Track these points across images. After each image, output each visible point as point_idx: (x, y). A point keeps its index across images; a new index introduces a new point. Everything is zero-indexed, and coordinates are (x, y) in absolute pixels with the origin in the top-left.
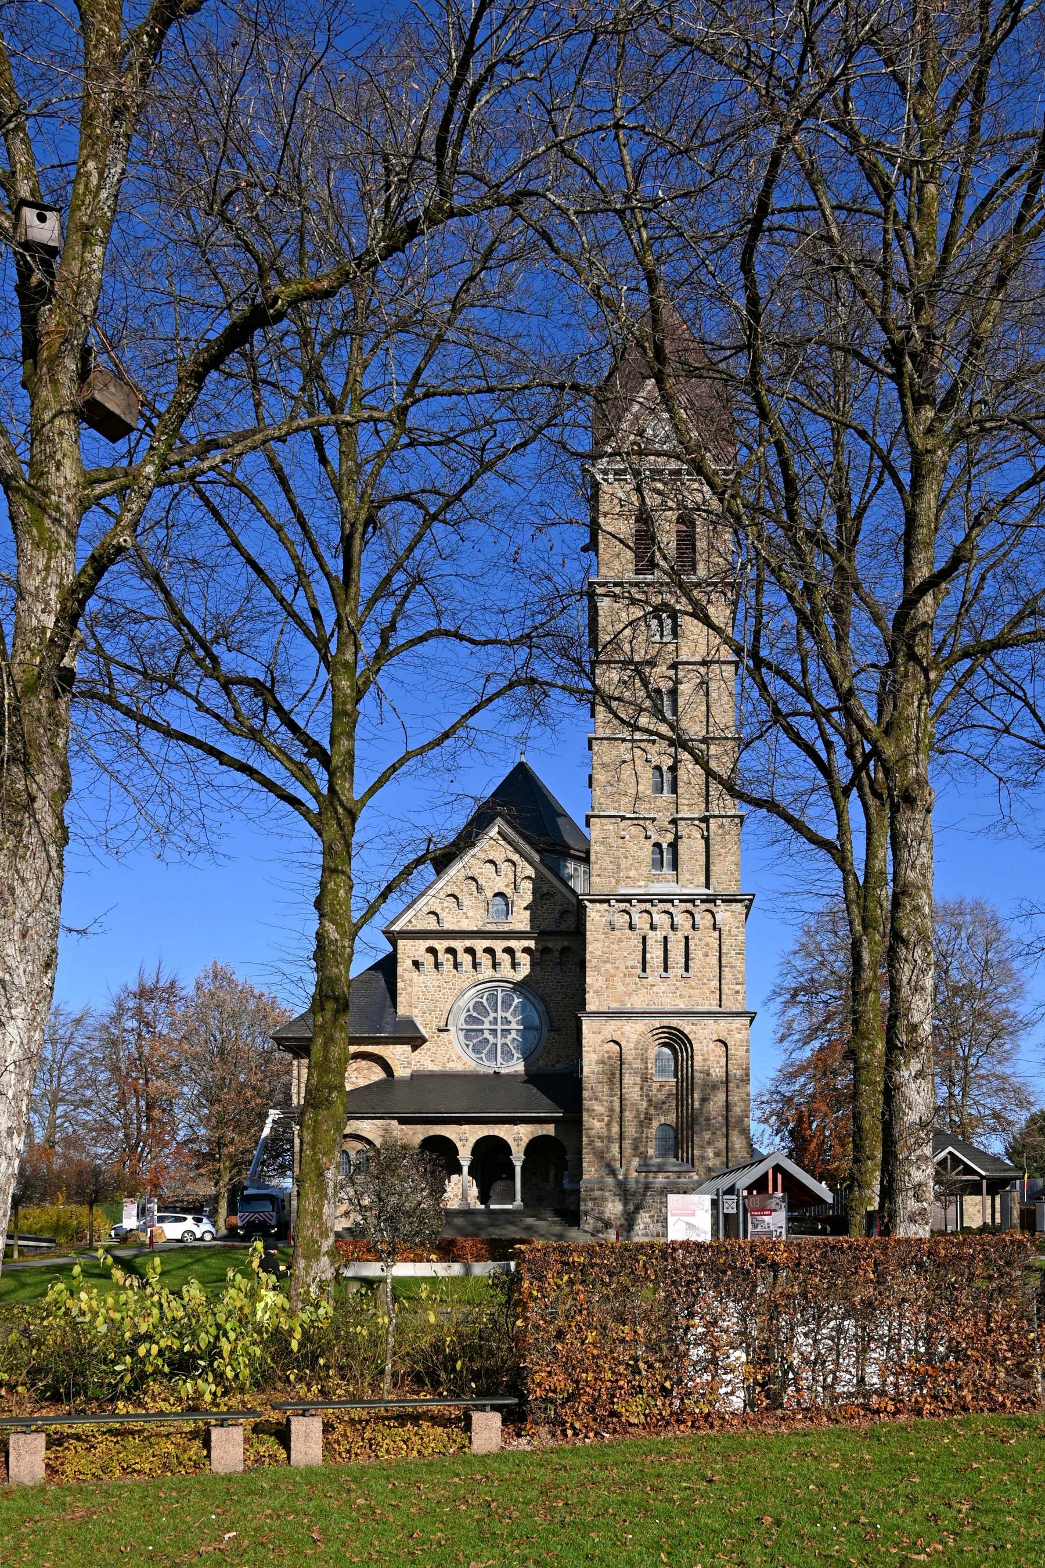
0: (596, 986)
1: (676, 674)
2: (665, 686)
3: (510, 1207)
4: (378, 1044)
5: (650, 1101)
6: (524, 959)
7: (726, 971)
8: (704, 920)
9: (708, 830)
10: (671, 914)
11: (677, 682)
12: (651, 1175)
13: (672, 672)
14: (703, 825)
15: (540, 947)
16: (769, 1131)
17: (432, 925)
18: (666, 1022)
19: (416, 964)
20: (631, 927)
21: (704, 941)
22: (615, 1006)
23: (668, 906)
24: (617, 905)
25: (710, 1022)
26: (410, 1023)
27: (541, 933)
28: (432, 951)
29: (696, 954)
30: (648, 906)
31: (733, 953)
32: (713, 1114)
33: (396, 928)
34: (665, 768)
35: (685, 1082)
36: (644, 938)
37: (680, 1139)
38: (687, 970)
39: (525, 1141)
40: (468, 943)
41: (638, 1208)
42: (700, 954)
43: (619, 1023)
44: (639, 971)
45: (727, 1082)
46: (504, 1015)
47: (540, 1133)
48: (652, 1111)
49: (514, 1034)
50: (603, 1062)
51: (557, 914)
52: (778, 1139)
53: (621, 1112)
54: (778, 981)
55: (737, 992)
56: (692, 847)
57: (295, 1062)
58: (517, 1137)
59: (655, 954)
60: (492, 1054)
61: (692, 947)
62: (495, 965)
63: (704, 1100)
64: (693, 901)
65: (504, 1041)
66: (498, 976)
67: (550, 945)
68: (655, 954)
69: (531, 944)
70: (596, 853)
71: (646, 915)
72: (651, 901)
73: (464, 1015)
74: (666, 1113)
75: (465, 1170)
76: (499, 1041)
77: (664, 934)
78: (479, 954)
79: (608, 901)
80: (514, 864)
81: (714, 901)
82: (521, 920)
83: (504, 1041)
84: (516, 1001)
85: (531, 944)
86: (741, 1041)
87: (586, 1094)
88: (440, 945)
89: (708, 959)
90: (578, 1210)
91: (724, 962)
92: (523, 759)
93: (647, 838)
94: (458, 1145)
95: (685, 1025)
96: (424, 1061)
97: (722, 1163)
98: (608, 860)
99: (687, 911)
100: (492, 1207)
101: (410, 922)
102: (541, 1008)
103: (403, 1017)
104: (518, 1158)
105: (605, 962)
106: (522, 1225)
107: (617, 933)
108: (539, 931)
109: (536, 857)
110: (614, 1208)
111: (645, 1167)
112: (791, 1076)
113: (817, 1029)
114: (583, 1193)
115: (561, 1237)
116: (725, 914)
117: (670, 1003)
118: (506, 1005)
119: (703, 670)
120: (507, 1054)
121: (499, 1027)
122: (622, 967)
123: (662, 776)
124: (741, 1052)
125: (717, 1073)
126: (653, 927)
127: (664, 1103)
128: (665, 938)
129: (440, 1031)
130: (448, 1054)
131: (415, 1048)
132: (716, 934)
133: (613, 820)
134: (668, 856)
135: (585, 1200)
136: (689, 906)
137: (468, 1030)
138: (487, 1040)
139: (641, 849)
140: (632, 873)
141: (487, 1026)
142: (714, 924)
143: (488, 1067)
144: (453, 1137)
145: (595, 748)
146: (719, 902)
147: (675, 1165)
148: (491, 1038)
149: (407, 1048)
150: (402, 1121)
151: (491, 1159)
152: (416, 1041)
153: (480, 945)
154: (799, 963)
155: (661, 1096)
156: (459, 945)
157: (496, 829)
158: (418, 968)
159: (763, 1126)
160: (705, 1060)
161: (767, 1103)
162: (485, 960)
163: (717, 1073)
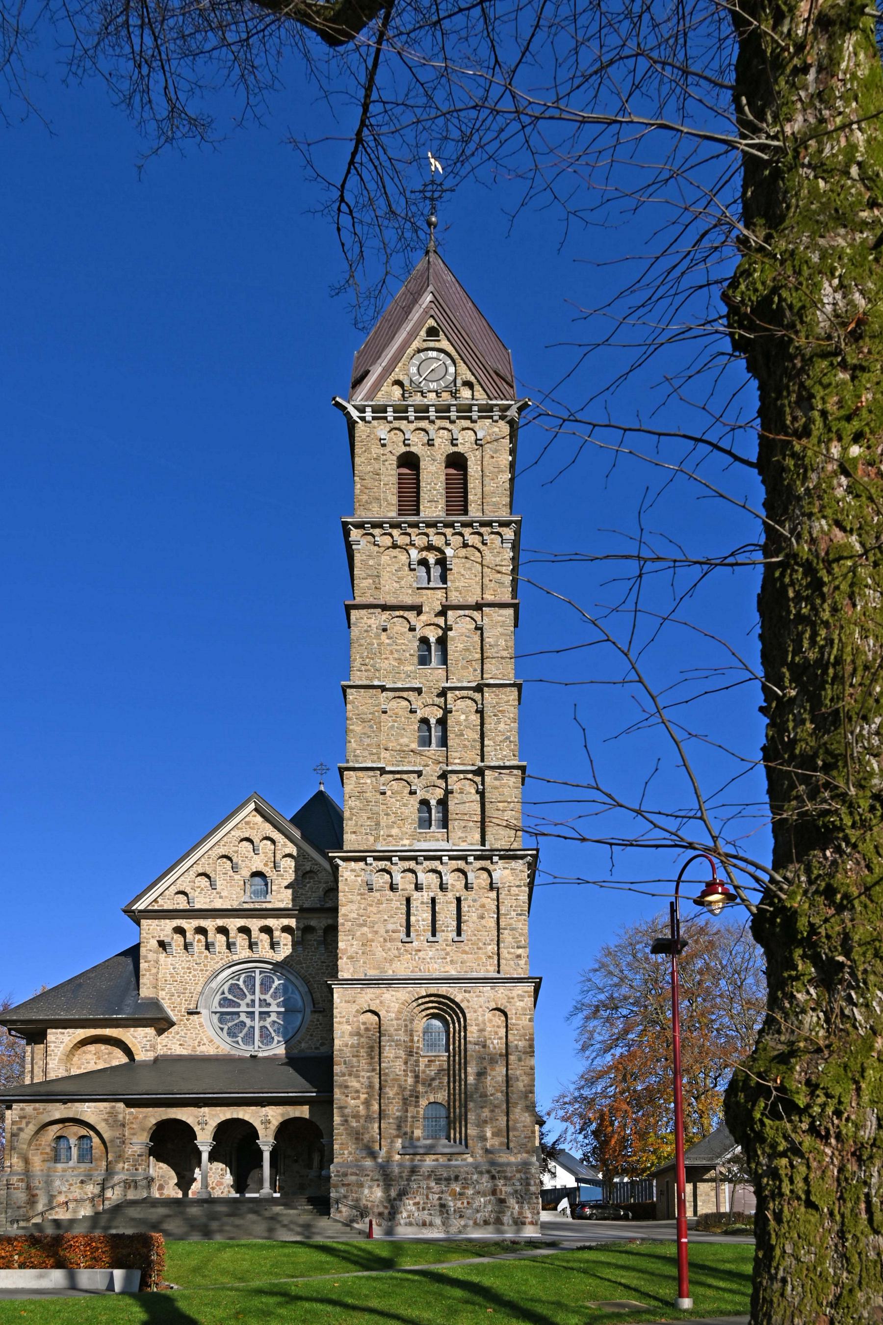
0: (351, 951)
1: (446, 621)
2: (433, 635)
3: (256, 1195)
4: (117, 1027)
5: (417, 1077)
6: (286, 940)
7: (506, 935)
8: (479, 880)
9: (483, 784)
10: (439, 873)
11: (448, 628)
12: (418, 1157)
13: (441, 621)
14: (478, 779)
15: (302, 926)
16: (571, 1129)
17: (181, 903)
18: (433, 989)
19: (162, 944)
20: (393, 888)
21: (478, 904)
22: (373, 973)
23: (436, 864)
24: (375, 864)
25: (487, 989)
26: (155, 1004)
27: (302, 910)
28: (180, 931)
29: (470, 915)
30: (412, 864)
31: (513, 914)
32: (490, 1090)
33: (141, 905)
34: (433, 721)
35: (458, 1056)
36: (408, 900)
37: (453, 1118)
38: (459, 934)
39: (275, 1123)
40: (220, 922)
41: (402, 1194)
42: (474, 916)
43: (378, 991)
44: (402, 935)
45: (507, 1054)
46: (263, 997)
47: (292, 1115)
48: (421, 1088)
49: (274, 1017)
50: (358, 1034)
51: (321, 893)
52: (581, 1137)
53: (380, 1089)
54: (580, 998)
55: (519, 956)
56: (465, 800)
57: (29, 1048)
58: (265, 1121)
59: (421, 917)
60: (249, 1038)
61: (465, 908)
62: (251, 946)
63: (481, 1074)
64: (464, 858)
65: (262, 1023)
66: (255, 956)
67: (313, 923)
68: (421, 917)
69: (292, 922)
70: (351, 808)
71: (410, 875)
72: (415, 858)
73: (218, 997)
74: (434, 1090)
76: (257, 1024)
77: (432, 894)
78: (233, 933)
79: (364, 859)
80: (273, 842)
81: (490, 858)
82: (282, 898)
83: (262, 1023)
84: (277, 982)
85: (292, 922)
86: (524, 1009)
87: (337, 1069)
88: (189, 925)
89: (483, 922)
90: (329, 1198)
91: (502, 924)
92: (322, 788)
93: (412, 793)
94: (197, 1129)
95: (457, 994)
96: (172, 1044)
97: (501, 1144)
98: (365, 815)
99: (459, 870)
100: (248, 1195)
101: (155, 901)
102: (304, 989)
104: (266, 1142)
105: (361, 925)
106: (267, 1214)
107: (377, 894)
108: (300, 910)
109: (297, 834)
110: (374, 1194)
111: (411, 1148)
112: (591, 1082)
113: (617, 1039)
114: (334, 1179)
115: (307, 1227)
116: (502, 872)
117: (436, 969)
119: (476, 615)
120: (266, 1037)
121: (257, 1009)
122: (382, 931)
123: (429, 730)
124: (524, 1021)
125: (497, 1044)
126: (418, 887)
127: (433, 1079)
128: (433, 900)
129: (190, 1013)
130: (199, 1036)
131: (160, 1032)
132: (493, 894)
133: (371, 773)
134: (437, 813)
135: (336, 1186)
136: (461, 864)
137: (222, 1013)
138: (243, 1024)
139: (405, 805)
140: (395, 831)
141: (243, 1008)
142: (491, 883)
143: (245, 1051)
145: (350, 697)
146: (496, 859)
147: (445, 1146)
148: (248, 1022)
149: (151, 1031)
150: (130, 1104)
151: (235, 1144)
152: (163, 1024)
153: (233, 924)
154: (599, 979)
155: (432, 1072)
156: (210, 924)
157: (252, 806)
158: (165, 949)
159: (565, 1124)
160: (481, 1031)
161: (570, 1103)
162: (241, 941)
163: (497, 1044)
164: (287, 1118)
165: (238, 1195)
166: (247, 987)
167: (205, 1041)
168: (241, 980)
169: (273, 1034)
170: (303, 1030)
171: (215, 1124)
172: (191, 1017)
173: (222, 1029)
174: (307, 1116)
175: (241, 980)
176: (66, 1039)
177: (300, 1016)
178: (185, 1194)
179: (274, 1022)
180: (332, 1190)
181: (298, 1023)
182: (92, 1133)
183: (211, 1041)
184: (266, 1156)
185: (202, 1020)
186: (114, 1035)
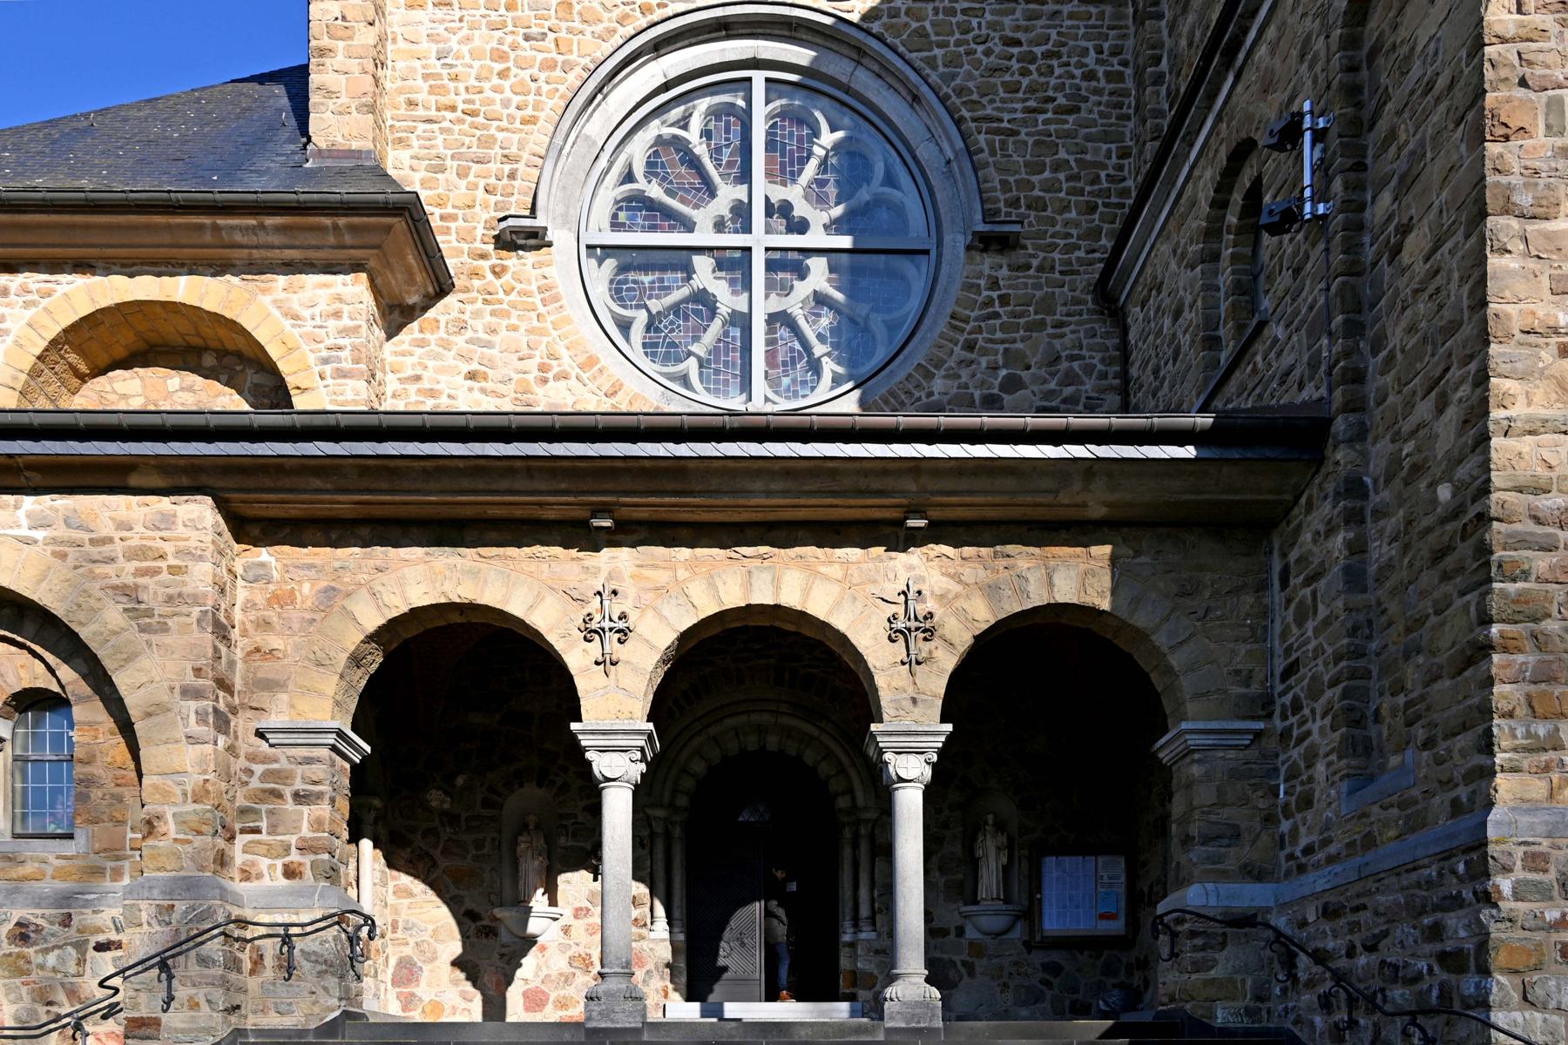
46: (778, 194)
49: (819, 275)
58: (901, 614)
73: (611, 192)
75: (618, 811)
83: (776, 304)
84: (828, 138)
94: (577, 657)
100: (732, 1010)
103: (331, 153)
118: (785, 170)
130: (531, 344)
131: (396, 314)
138: (704, 300)
141: (704, 236)
144: (552, 620)
164: (1014, 607)
165: (690, 1011)
166: (716, 153)
167: (567, 362)
168: (696, 123)
169: (819, 349)
170: (937, 324)
171: (666, 638)
172: (512, 260)
173: (625, 326)
174: (1105, 605)
175: (696, 123)
176: (17, 317)
177: (916, 275)
178: (495, 1007)
179: (820, 299)
180: (1502, 985)
181: (914, 304)
182: (66, 673)
183: (591, 362)
184: (910, 805)
185: (549, 271)
186: (210, 305)
